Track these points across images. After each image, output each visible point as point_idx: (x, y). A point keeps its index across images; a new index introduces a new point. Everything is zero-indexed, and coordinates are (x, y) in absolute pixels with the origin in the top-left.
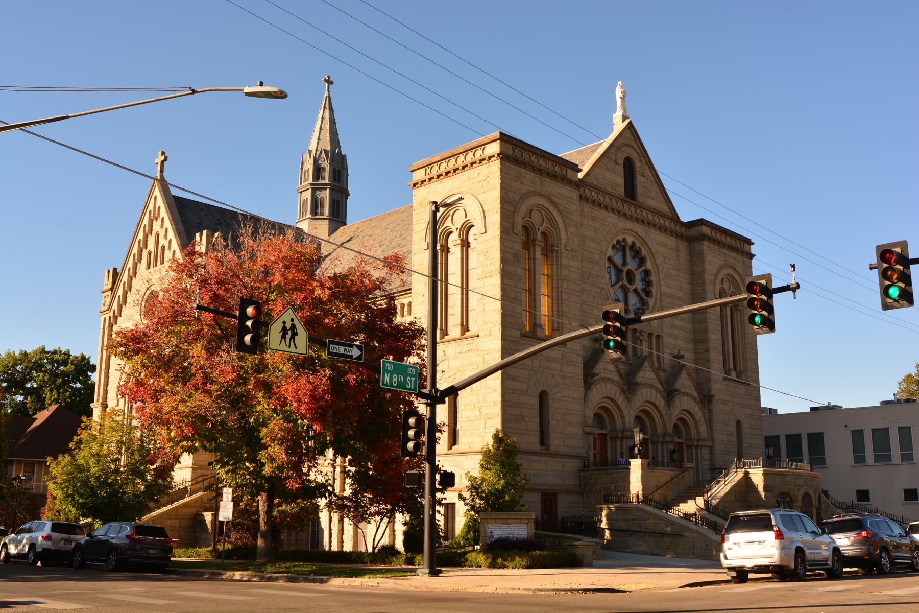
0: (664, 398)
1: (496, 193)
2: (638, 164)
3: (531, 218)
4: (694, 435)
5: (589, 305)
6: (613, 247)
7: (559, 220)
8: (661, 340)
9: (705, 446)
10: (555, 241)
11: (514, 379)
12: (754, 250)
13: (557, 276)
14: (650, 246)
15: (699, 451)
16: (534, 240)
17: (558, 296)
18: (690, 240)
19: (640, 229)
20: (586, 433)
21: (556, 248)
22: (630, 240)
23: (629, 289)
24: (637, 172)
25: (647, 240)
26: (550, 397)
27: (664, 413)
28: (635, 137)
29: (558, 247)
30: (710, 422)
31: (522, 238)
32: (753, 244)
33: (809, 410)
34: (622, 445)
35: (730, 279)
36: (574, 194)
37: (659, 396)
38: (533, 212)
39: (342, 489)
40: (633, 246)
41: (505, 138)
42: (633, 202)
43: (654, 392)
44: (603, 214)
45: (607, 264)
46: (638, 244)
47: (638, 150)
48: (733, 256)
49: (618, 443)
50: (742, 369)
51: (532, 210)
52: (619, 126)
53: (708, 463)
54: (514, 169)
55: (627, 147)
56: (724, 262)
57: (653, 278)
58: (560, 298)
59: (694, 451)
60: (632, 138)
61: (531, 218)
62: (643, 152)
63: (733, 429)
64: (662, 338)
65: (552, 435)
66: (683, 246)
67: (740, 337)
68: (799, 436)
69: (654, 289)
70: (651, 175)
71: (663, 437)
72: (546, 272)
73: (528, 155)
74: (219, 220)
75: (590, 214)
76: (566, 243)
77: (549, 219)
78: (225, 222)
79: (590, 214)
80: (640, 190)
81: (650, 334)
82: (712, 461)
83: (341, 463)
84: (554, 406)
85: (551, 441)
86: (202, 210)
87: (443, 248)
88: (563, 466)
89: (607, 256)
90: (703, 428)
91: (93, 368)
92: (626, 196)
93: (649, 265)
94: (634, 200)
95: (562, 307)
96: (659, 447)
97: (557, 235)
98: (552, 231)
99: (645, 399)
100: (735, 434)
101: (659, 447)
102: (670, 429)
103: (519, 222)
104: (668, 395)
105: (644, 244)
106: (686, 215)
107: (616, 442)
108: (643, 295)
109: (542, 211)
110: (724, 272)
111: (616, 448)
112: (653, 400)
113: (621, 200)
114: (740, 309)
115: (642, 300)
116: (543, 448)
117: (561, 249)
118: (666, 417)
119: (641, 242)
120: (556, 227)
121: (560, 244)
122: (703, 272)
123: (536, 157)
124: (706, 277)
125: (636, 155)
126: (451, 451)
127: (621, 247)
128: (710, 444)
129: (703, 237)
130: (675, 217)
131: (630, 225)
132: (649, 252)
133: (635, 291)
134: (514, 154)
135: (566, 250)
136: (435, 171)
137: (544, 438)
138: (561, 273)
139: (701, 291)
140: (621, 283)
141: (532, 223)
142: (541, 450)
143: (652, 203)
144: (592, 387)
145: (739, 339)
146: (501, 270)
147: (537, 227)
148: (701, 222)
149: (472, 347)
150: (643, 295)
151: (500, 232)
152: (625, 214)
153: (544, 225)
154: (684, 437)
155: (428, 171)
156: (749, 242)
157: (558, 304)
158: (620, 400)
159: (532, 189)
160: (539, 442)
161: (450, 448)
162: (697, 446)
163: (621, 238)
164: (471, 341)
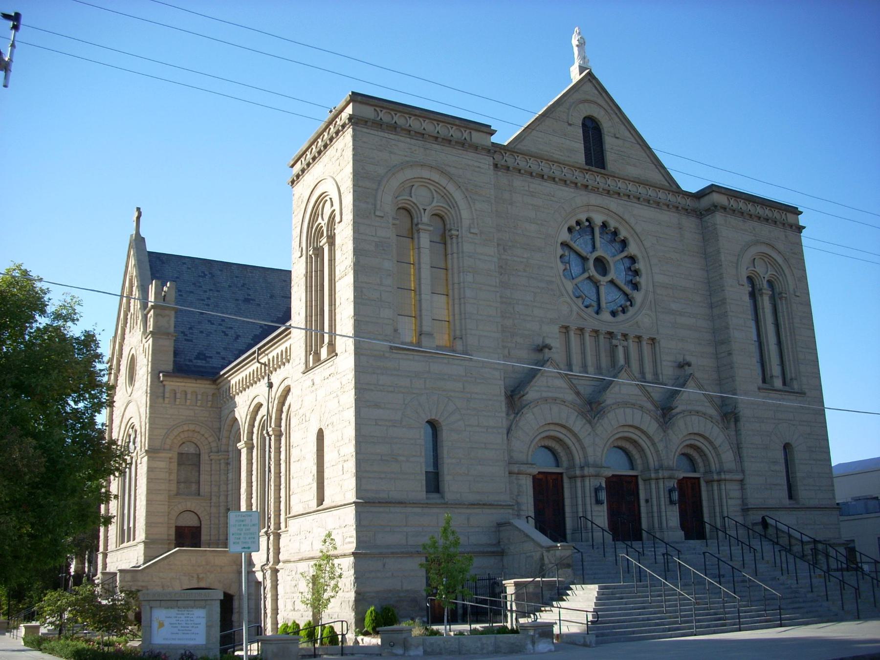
0: (657, 420)
1: (349, 169)
2: (606, 125)
3: (755, 268)
4: (714, 466)
5: (528, 305)
6: (570, 230)
7: (458, 196)
8: (657, 344)
10: (782, 288)
11: (377, 406)
12: (802, 220)
13: (459, 268)
14: (632, 225)
15: (723, 487)
16: (760, 290)
18: (700, 214)
19: (613, 204)
21: (784, 295)
22: (598, 219)
24: (605, 133)
25: (626, 217)
26: (444, 428)
27: (656, 441)
28: (600, 89)
29: (786, 294)
30: (738, 449)
31: (748, 288)
32: (801, 213)
34: (583, 487)
35: (766, 260)
36: (486, 162)
37: (647, 418)
38: (756, 260)
39: (277, 561)
41: (359, 98)
42: (602, 171)
43: (638, 414)
44: (549, 187)
45: (560, 252)
46: (613, 224)
47: (606, 106)
48: (765, 231)
49: (579, 484)
50: (793, 375)
51: (754, 259)
52: (575, 76)
53: (739, 502)
54: (376, 137)
55: (586, 104)
56: (754, 238)
57: (641, 265)
58: (462, 296)
59: (715, 487)
60: (596, 92)
61: (411, 197)
62: (614, 108)
63: (780, 455)
64: (659, 342)
66: (690, 223)
67: (788, 334)
69: (643, 280)
70: (630, 136)
72: (412, 260)
73: (778, 213)
74: (203, 272)
75: (527, 188)
76: (794, 289)
77: (773, 266)
78: (210, 273)
79: (527, 188)
80: (610, 157)
81: (639, 338)
82: (743, 499)
83: (275, 529)
84: (447, 437)
86: (184, 263)
87: (317, 252)
88: (468, 519)
89: (560, 242)
90: (728, 456)
92: (587, 164)
93: (633, 249)
94: (604, 168)
96: (653, 486)
97: (457, 216)
98: (778, 278)
99: (623, 423)
101: (653, 486)
103: (387, 203)
104: (664, 415)
105: (624, 222)
106: (691, 184)
107: (712, 486)
108: (628, 289)
109: (764, 258)
110: (753, 250)
111: (651, 492)
112: (637, 424)
113: (579, 168)
114: (786, 298)
116: (792, 502)
117: (462, 233)
118: (661, 446)
120: (454, 205)
121: (462, 227)
122: (718, 252)
123: (761, 207)
124: (723, 259)
125: (603, 113)
126: (320, 508)
127: (586, 227)
128: (739, 477)
129: (715, 208)
130: (674, 187)
131: (595, 199)
132: (633, 232)
134: (729, 204)
135: (471, 233)
136: (309, 156)
137: (434, 483)
140: (586, 275)
141: (414, 203)
142: (790, 504)
143: (632, 171)
144: (525, 410)
145: (786, 336)
146: (354, 264)
147: (762, 276)
148: (712, 189)
149: (332, 370)
150: (628, 289)
151: (352, 216)
152: (586, 187)
153: (769, 273)
154: (702, 470)
155: (303, 160)
156: (796, 212)
158: (578, 425)
159: (407, 159)
161: (318, 506)
162: (719, 481)
163: (583, 217)
164: (332, 363)
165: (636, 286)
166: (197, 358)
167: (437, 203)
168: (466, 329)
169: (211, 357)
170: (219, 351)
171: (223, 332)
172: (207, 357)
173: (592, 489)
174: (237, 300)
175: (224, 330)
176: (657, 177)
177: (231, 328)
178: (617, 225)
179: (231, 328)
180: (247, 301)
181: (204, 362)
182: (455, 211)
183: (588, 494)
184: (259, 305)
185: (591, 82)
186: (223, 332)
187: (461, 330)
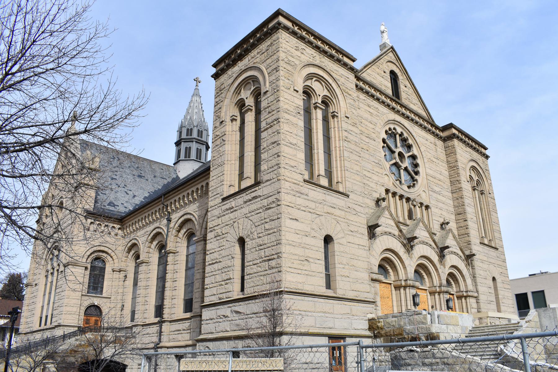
9: (472, 297)
13: (339, 137)
17: (340, 154)
20: (372, 280)
22: (399, 130)
23: (401, 166)
33: (528, 276)
40: (401, 135)
45: (382, 144)
46: (405, 135)
47: (399, 66)
48: (476, 155)
57: (419, 161)
65: (338, 278)
66: (440, 143)
68: (526, 294)
69: (420, 169)
71: (440, 286)
74: (113, 156)
78: (117, 158)
85: (337, 284)
91: (344, 341)
95: (344, 164)
100: (493, 287)
102: (444, 282)
115: (412, 178)
119: (407, 133)
133: (406, 169)
138: (342, 135)
139: (456, 176)
148: (451, 126)
157: (341, 160)
160: (325, 285)
165: (417, 173)
166: (109, 204)
167: (326, 93)
168: (345, 177)
169: (118, 206)
170: (123, 202)
171: (125, 192)
172: (116, 205)
173: (411, 295)
174: (134, 175)
175: (126, 191)
176: (423, 114)
177: (131, 190)
178: (407, 136)
179: (131, 190)
180: (140, 176)
181: (113, 208)
182: (336, 101)
183: (408, 298)
184: (147, 180)
185: (393, 52)
186: (125, 192)
187: (342, 178)
